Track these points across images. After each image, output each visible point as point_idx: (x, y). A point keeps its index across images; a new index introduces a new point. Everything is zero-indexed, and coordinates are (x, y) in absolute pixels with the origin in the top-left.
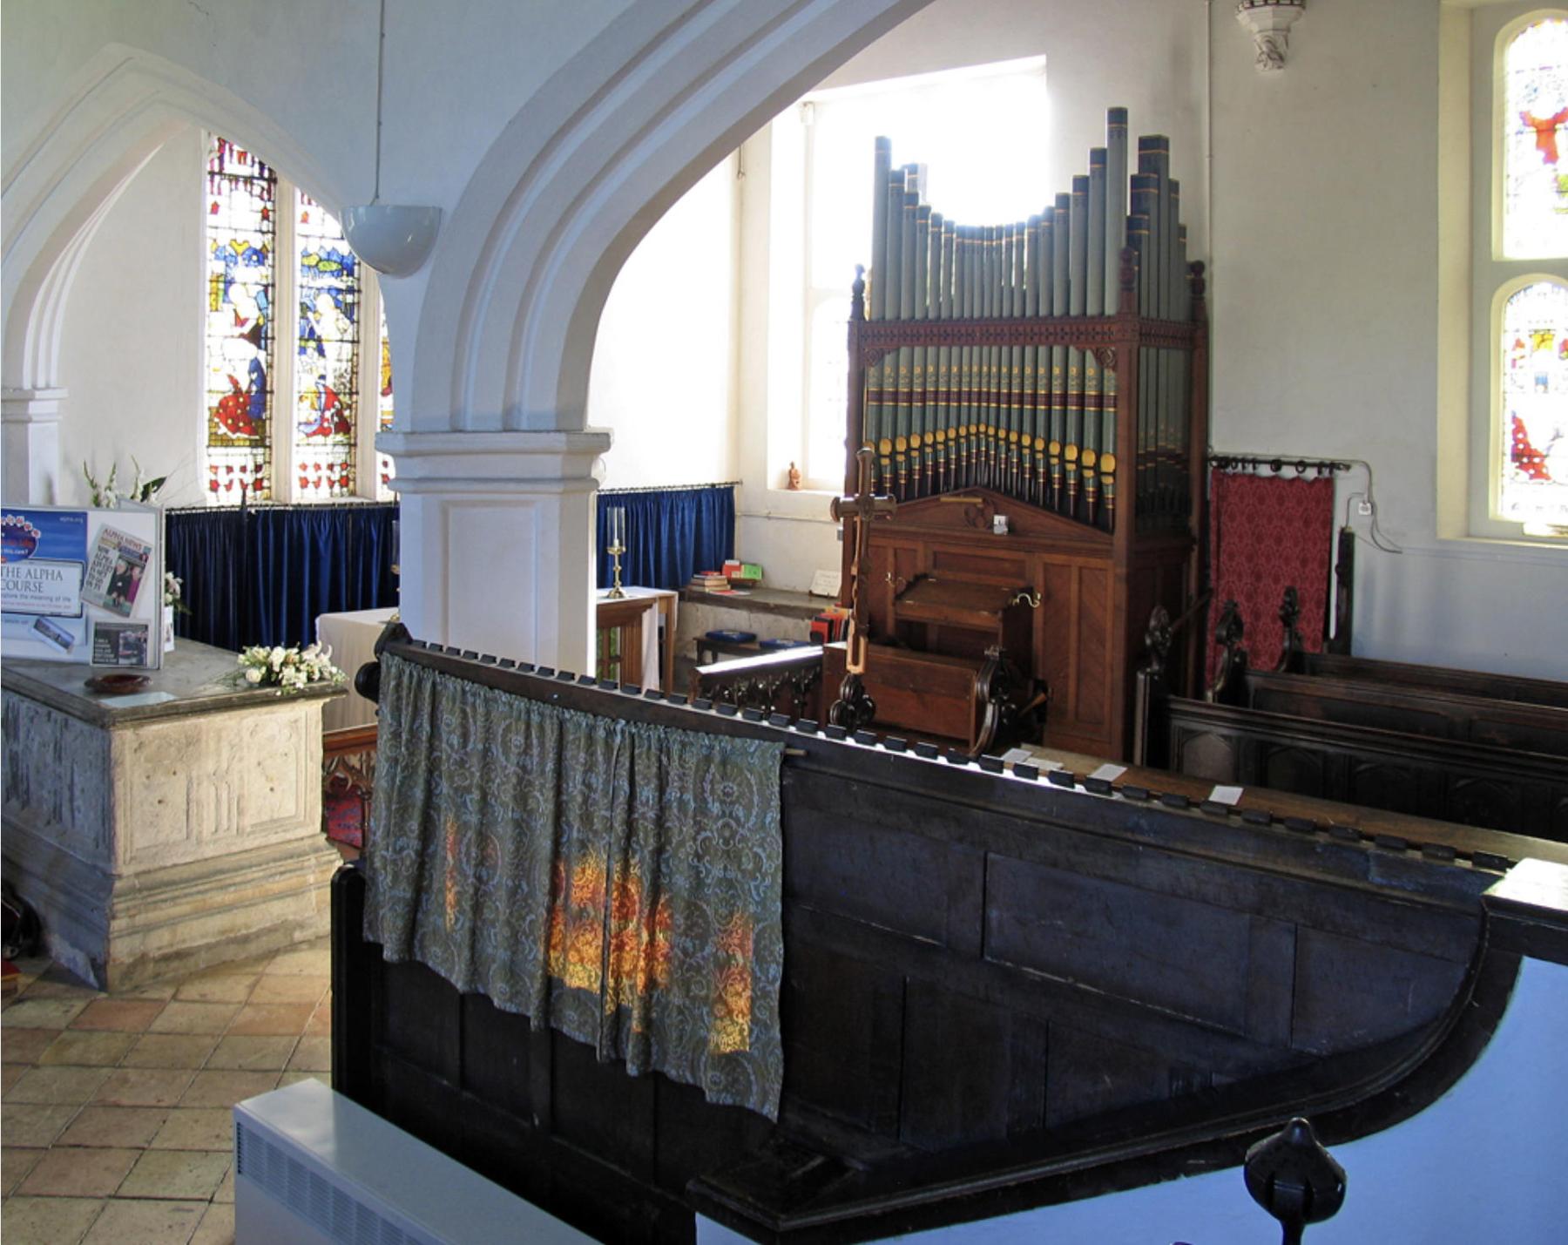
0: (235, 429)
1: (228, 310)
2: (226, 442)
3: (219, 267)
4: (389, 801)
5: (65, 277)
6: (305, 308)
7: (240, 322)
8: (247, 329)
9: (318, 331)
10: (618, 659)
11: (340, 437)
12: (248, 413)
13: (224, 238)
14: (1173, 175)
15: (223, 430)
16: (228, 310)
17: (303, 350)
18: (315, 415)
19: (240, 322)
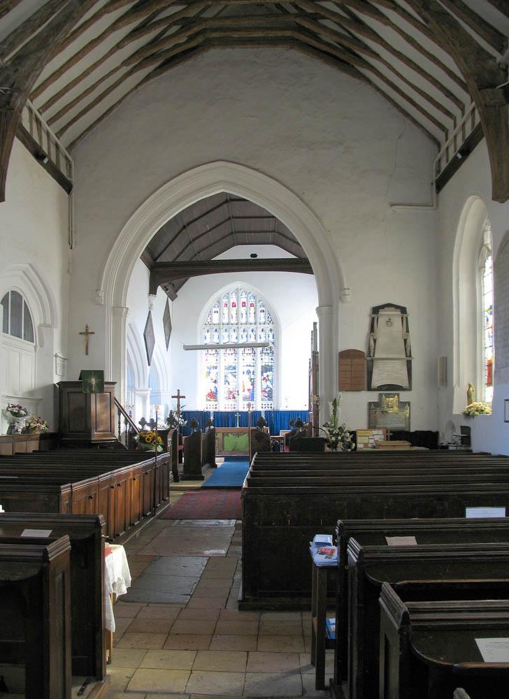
1: (210, 378)
10: (234, 305)
12: (213, 395)
15: (209, 398)
16: (210, 378)
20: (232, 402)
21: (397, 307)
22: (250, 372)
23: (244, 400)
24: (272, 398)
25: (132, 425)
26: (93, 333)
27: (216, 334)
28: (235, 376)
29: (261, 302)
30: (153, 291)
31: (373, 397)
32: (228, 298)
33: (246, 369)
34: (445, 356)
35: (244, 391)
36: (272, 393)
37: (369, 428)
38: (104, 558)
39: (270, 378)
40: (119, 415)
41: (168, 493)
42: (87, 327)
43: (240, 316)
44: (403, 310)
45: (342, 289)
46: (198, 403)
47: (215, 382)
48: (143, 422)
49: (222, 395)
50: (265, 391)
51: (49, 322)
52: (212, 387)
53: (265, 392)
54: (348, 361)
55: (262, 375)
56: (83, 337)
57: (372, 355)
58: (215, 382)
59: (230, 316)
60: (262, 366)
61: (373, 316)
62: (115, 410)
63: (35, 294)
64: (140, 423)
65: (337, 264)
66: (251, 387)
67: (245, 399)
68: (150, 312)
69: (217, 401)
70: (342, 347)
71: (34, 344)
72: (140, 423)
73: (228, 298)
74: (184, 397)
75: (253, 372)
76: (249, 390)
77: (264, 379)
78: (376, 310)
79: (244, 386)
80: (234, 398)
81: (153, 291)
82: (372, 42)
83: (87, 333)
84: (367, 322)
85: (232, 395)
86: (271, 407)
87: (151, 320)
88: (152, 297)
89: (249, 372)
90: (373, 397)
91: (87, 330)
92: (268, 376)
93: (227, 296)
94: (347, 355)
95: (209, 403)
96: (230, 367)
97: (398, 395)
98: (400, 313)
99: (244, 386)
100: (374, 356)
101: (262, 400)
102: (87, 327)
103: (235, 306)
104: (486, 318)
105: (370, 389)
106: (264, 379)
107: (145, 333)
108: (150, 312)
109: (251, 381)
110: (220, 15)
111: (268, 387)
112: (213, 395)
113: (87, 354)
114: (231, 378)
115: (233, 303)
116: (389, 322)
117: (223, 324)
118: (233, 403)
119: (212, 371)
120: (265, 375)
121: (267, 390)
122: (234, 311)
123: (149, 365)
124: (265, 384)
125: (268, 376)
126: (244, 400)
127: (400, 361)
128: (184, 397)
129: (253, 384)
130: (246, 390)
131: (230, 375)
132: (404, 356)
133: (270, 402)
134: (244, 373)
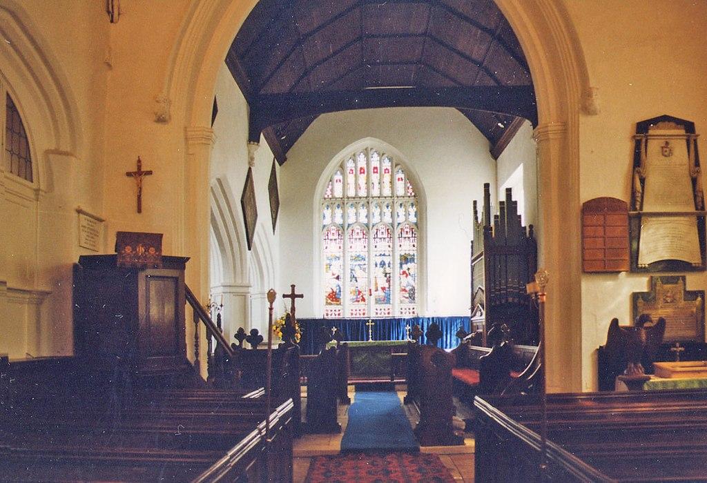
0: (332, 301)
1: (330, 273)
2: (330, 304)
3: (328, 262)
4: (634, 424)
5: (224, 221)
6: (352, 270)
7: (333, 275)
8: (335, 276)
9: (356, 276)
10: (362, 171)
11: (363, 302)
12: (334, 297)
13: (329, 255)
14: (591, 86)
15: (329, 301)
16: (330, 273)
17: (351, 281)
18: (355, 297)
19: (333, 275)
21: (679, 122)
22: (384, 264)
23: (377, 303)
24: (414, 299)
25: (222, 342)
26: (150, 173)
27: (339, 212)
29: (399, 167)
30: (253, 138)
31: (641, 284)
32: (355, 161)
33: (379, 260)
35: (377, 290)
36: (414, 293)
39: (412, 272)
40: (196, 322)
42: (139, 161)
43: (371, 186)
44: (689, 127)
45: (587, 94)
46: (315, 308)
47: (338, 278)
48: (240, 335)
49: (347, 297)
50: (405, 290)
51: (65, 147)
52: (333, 285)
53: (406, 291)
54: (596, 219)
55: (401, 267)
56: (131, 181)
57: (638, 207)
58: (338, 278)
59: (357, 187)
60: (401, 256)
61: (639, 136)
62: (188, 310)
63: (39, 93)
64: (236, 336)
65: (575, 41)
66: (386, 285)
67: (378, 301)
68: (250, 169)
70: (587, 193)
71: (34, 185)
72: (236, 336)
73: (355, 161)
74: (301, 296)
75: (389, 264)
76: (383, 289)
77: (404, 273)
78: (642, 128)
79: (376, 284)
80: (363, 300)
81: (253, 138)
83: (139, 173)
84: (627, 148)
85: (360, 297)
86: (414, 313)
87: (252, 182)
88: (253, 146)
89: (383, 264)
90: (641, 284)
91: (139, 167)
92: (409, 269)
93: (354, 158)
94: (596, 207)
95: (329, 307)
96: (358, 256)
97: (684, 279)
98: (683, 132)
99: (376, 284)
100: (641, 208)
101: (401, 302)
102: (139, 161)
103: (364, 173)
104: (416, 281)
105: (635, 269)
106: (404, 273)
107: (243, 198)
108: (250, 169)
109: (386, 276)
113: (139, 211)
115: (361, 169)
116: (666, 150)
117: (348, 198)
119: (334, 263)
120: (405, 267)
121: (407, 289)
122: (362, 179)
123: (250, 249)
124: (406, 281)
125: (409, 269)
126: (377, 303)
127: (686, 219)
128: (301, 296)
129: (388, 281)
130: (379, 289)
131: (357, 268)
132: (692, 209)
133: (411, 306)
134: (376, 265)
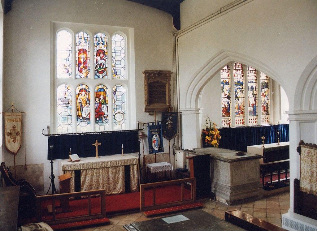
12: (227, 111)
20: (240, 117)
28: (242, 92)
34: (302, 140)
37: (264, 197)
38: (181, 214)
41: (262, 91)
47: (228, 97)
69: (229, 116)
80: (242, 113)
82: (200, 123)
110: (141, 169)
111: (265, 102)
112: (227, 111)
114: (240, 94)
118: (242, 118)
119: (226, 86)
125: (265, 92)
129: (255, 100)
130: (251, 105)
131: (238, 91)
